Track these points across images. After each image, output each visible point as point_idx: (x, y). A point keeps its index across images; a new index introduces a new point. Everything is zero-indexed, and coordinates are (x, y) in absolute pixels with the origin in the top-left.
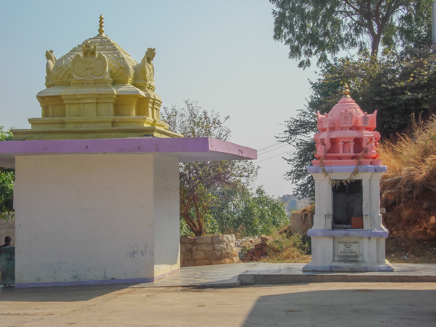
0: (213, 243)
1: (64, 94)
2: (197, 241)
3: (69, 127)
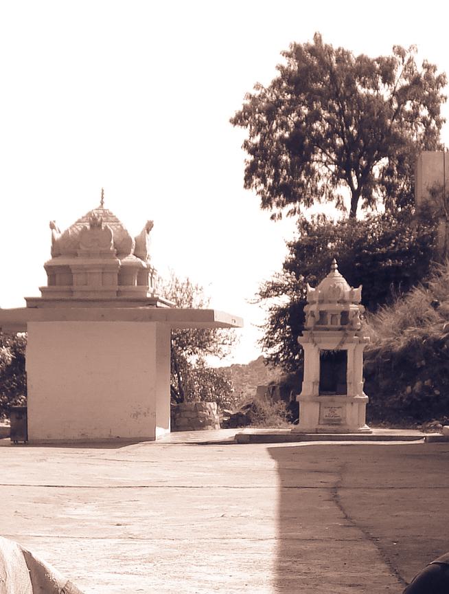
0: (196, 411)
1: (73, 264)
2: (180, 408)
3: (77, 296)
